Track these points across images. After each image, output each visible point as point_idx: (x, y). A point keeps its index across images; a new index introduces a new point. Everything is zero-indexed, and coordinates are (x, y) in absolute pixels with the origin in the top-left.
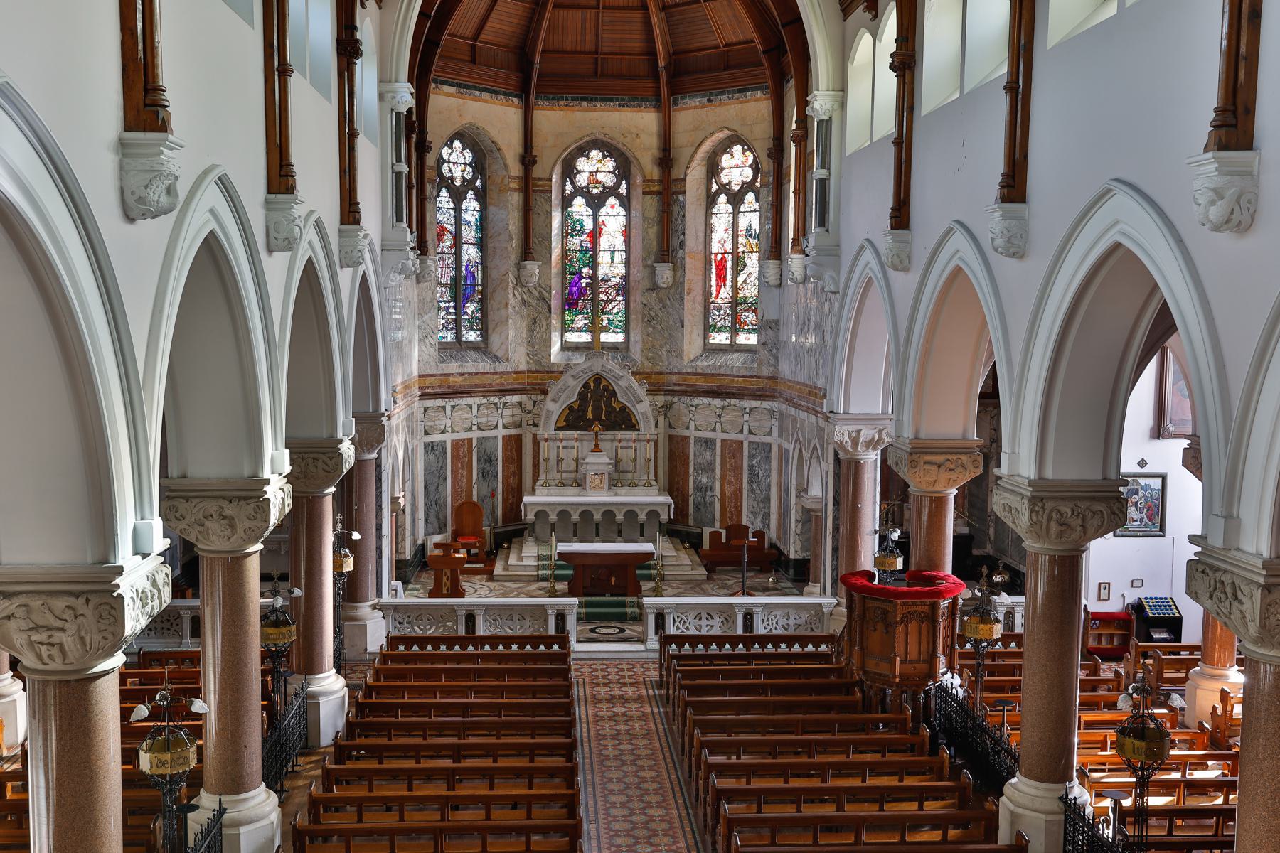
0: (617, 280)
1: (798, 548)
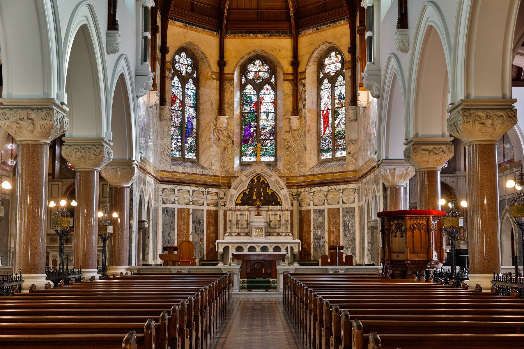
0: (270, 128)
1: (370, 258)
